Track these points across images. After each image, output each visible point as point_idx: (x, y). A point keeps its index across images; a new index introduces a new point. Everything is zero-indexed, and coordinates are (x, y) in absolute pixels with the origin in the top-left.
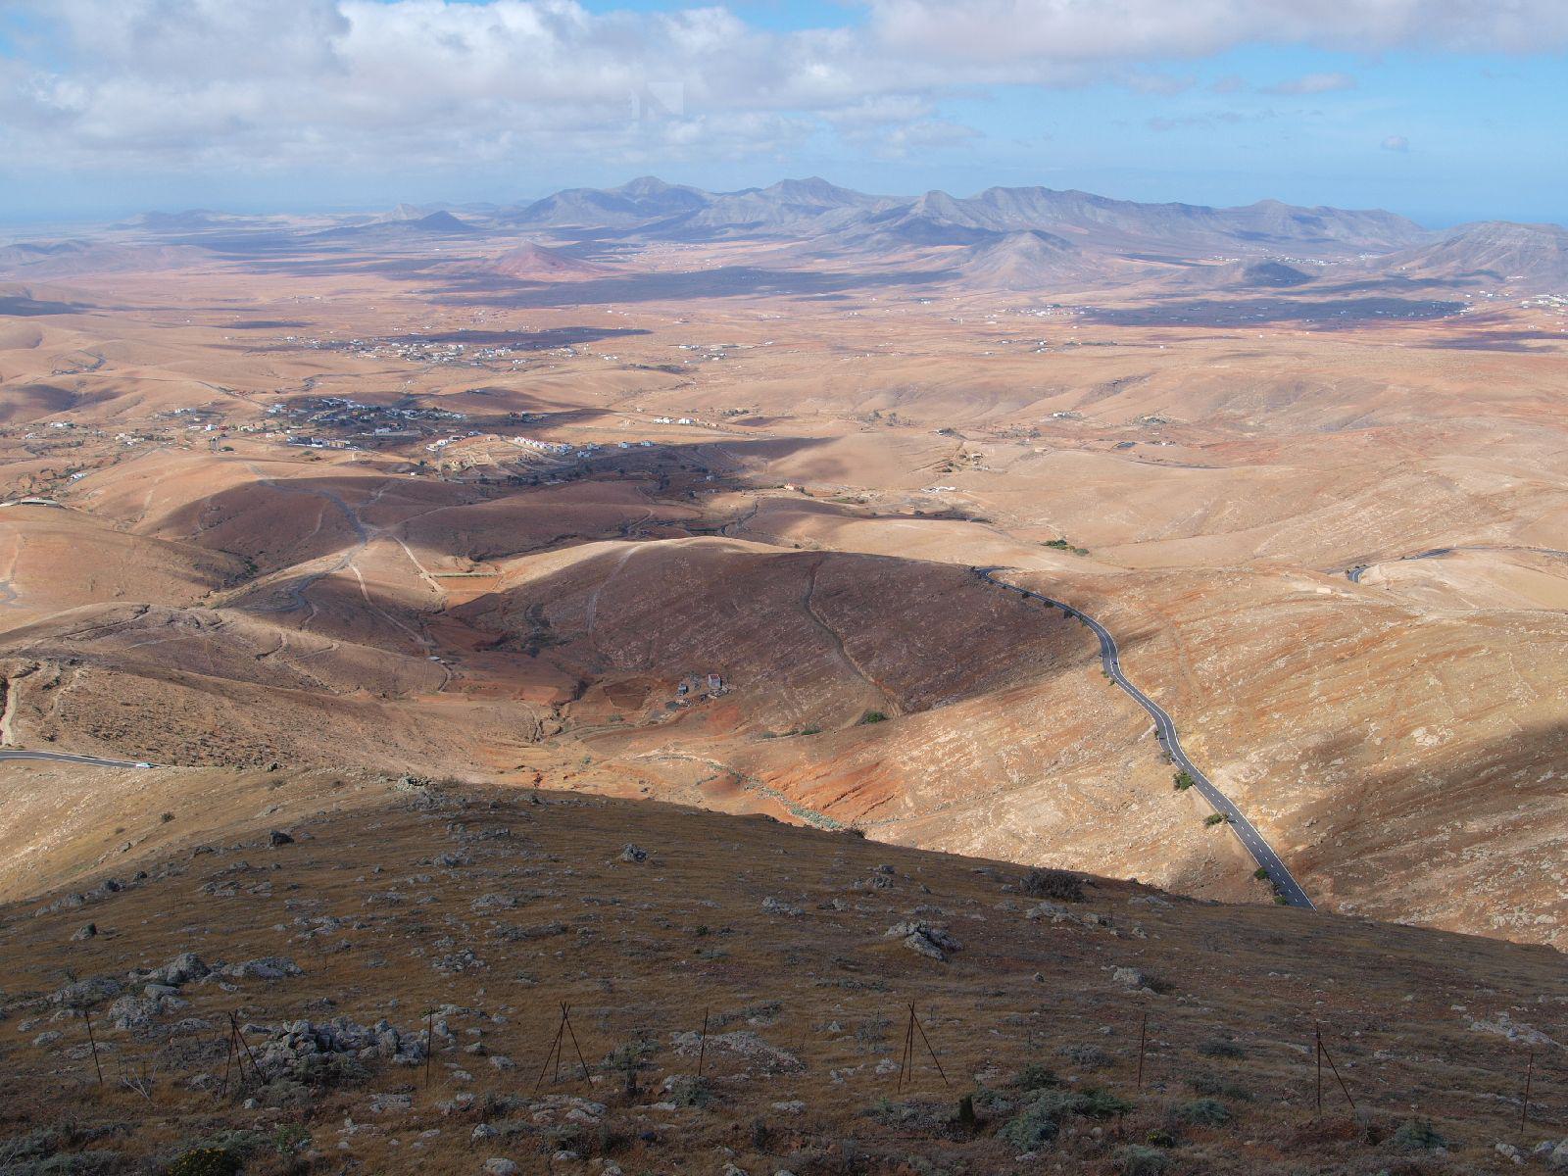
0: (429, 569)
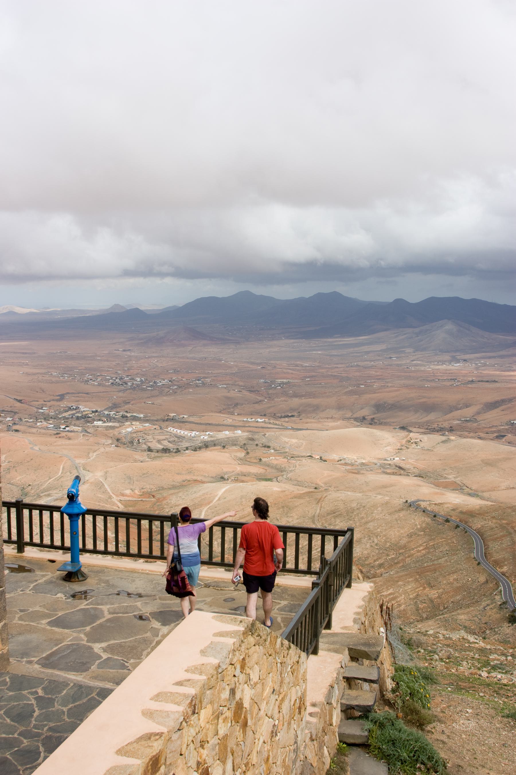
0: (117, 496)
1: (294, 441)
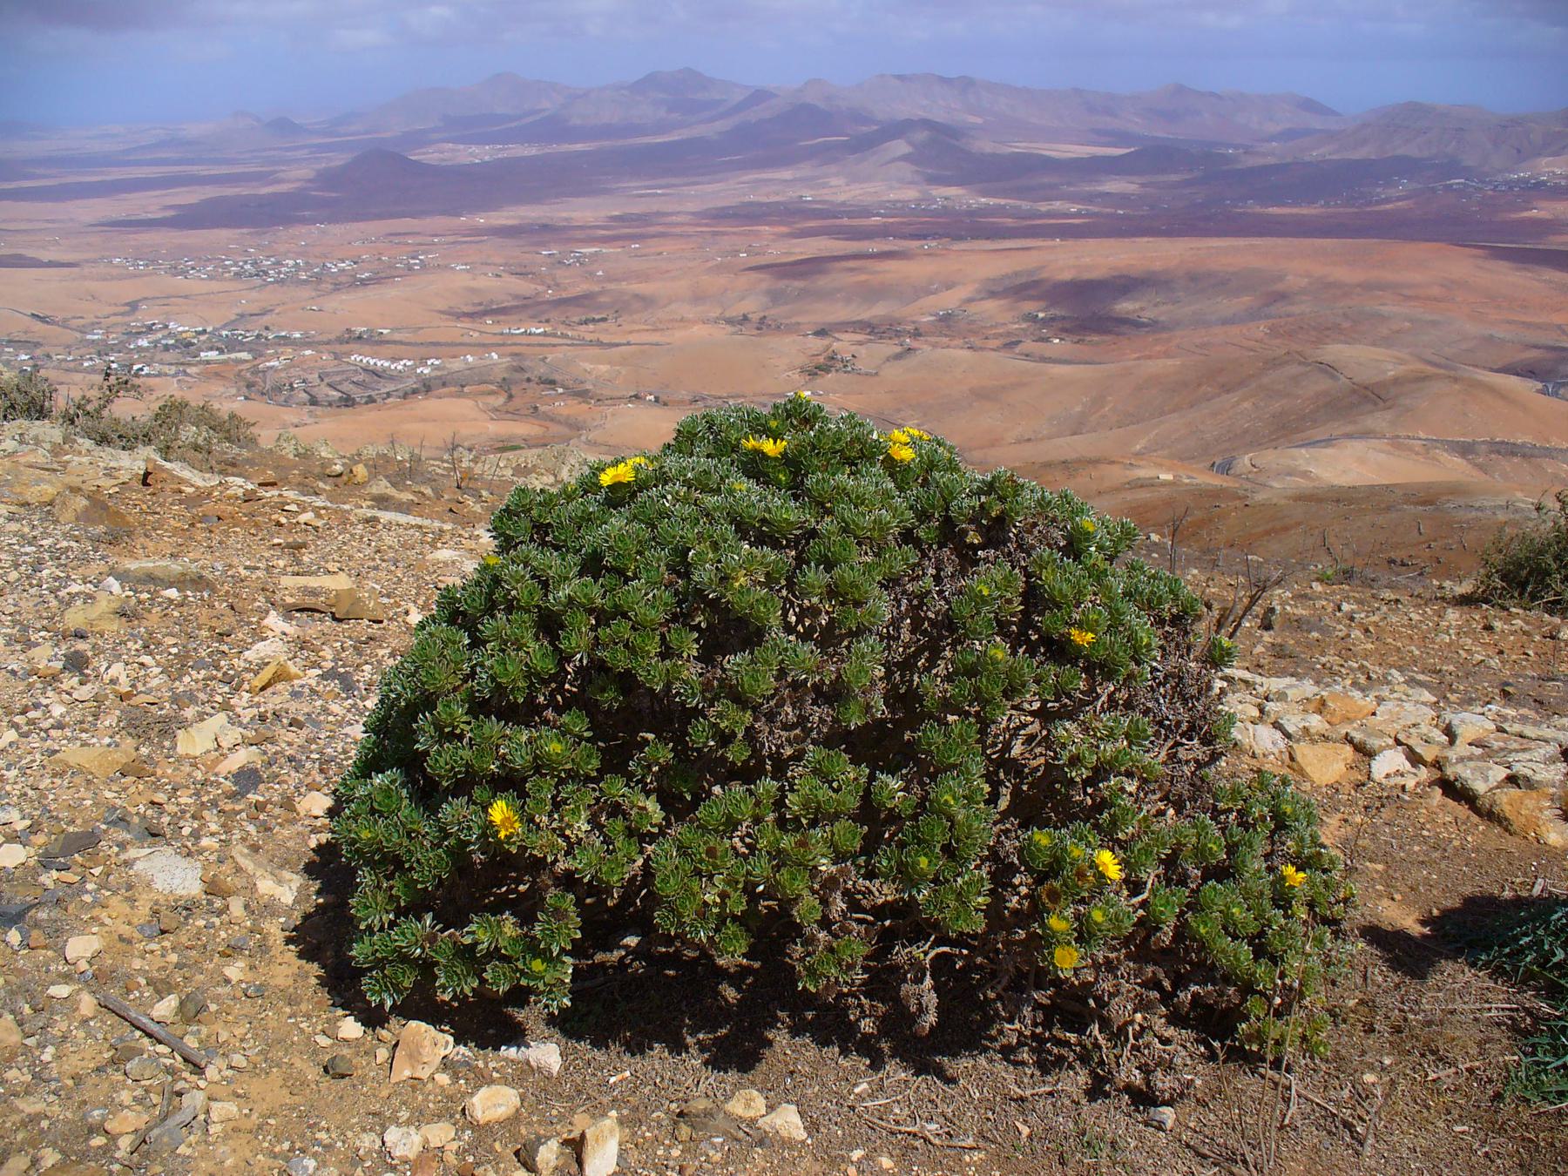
1: (604, 368)
